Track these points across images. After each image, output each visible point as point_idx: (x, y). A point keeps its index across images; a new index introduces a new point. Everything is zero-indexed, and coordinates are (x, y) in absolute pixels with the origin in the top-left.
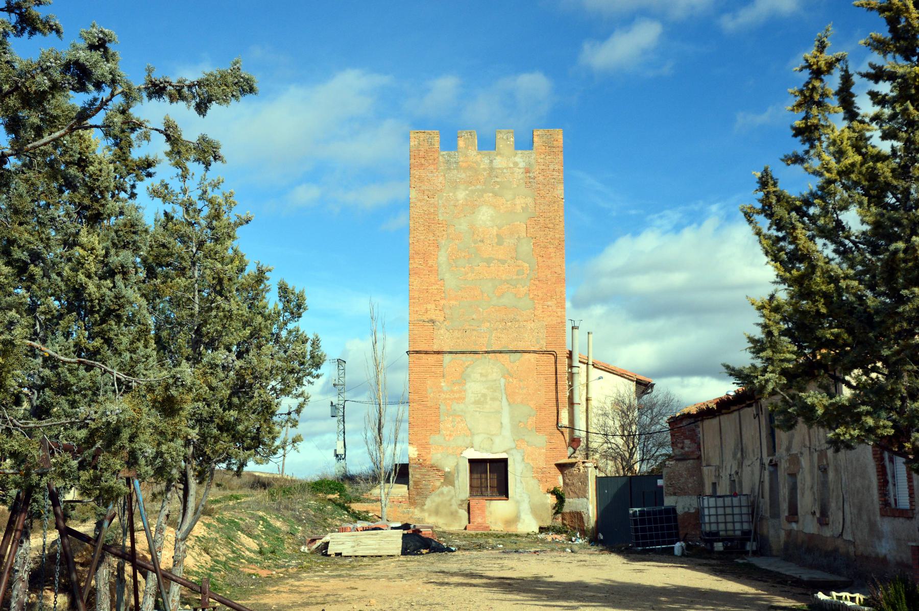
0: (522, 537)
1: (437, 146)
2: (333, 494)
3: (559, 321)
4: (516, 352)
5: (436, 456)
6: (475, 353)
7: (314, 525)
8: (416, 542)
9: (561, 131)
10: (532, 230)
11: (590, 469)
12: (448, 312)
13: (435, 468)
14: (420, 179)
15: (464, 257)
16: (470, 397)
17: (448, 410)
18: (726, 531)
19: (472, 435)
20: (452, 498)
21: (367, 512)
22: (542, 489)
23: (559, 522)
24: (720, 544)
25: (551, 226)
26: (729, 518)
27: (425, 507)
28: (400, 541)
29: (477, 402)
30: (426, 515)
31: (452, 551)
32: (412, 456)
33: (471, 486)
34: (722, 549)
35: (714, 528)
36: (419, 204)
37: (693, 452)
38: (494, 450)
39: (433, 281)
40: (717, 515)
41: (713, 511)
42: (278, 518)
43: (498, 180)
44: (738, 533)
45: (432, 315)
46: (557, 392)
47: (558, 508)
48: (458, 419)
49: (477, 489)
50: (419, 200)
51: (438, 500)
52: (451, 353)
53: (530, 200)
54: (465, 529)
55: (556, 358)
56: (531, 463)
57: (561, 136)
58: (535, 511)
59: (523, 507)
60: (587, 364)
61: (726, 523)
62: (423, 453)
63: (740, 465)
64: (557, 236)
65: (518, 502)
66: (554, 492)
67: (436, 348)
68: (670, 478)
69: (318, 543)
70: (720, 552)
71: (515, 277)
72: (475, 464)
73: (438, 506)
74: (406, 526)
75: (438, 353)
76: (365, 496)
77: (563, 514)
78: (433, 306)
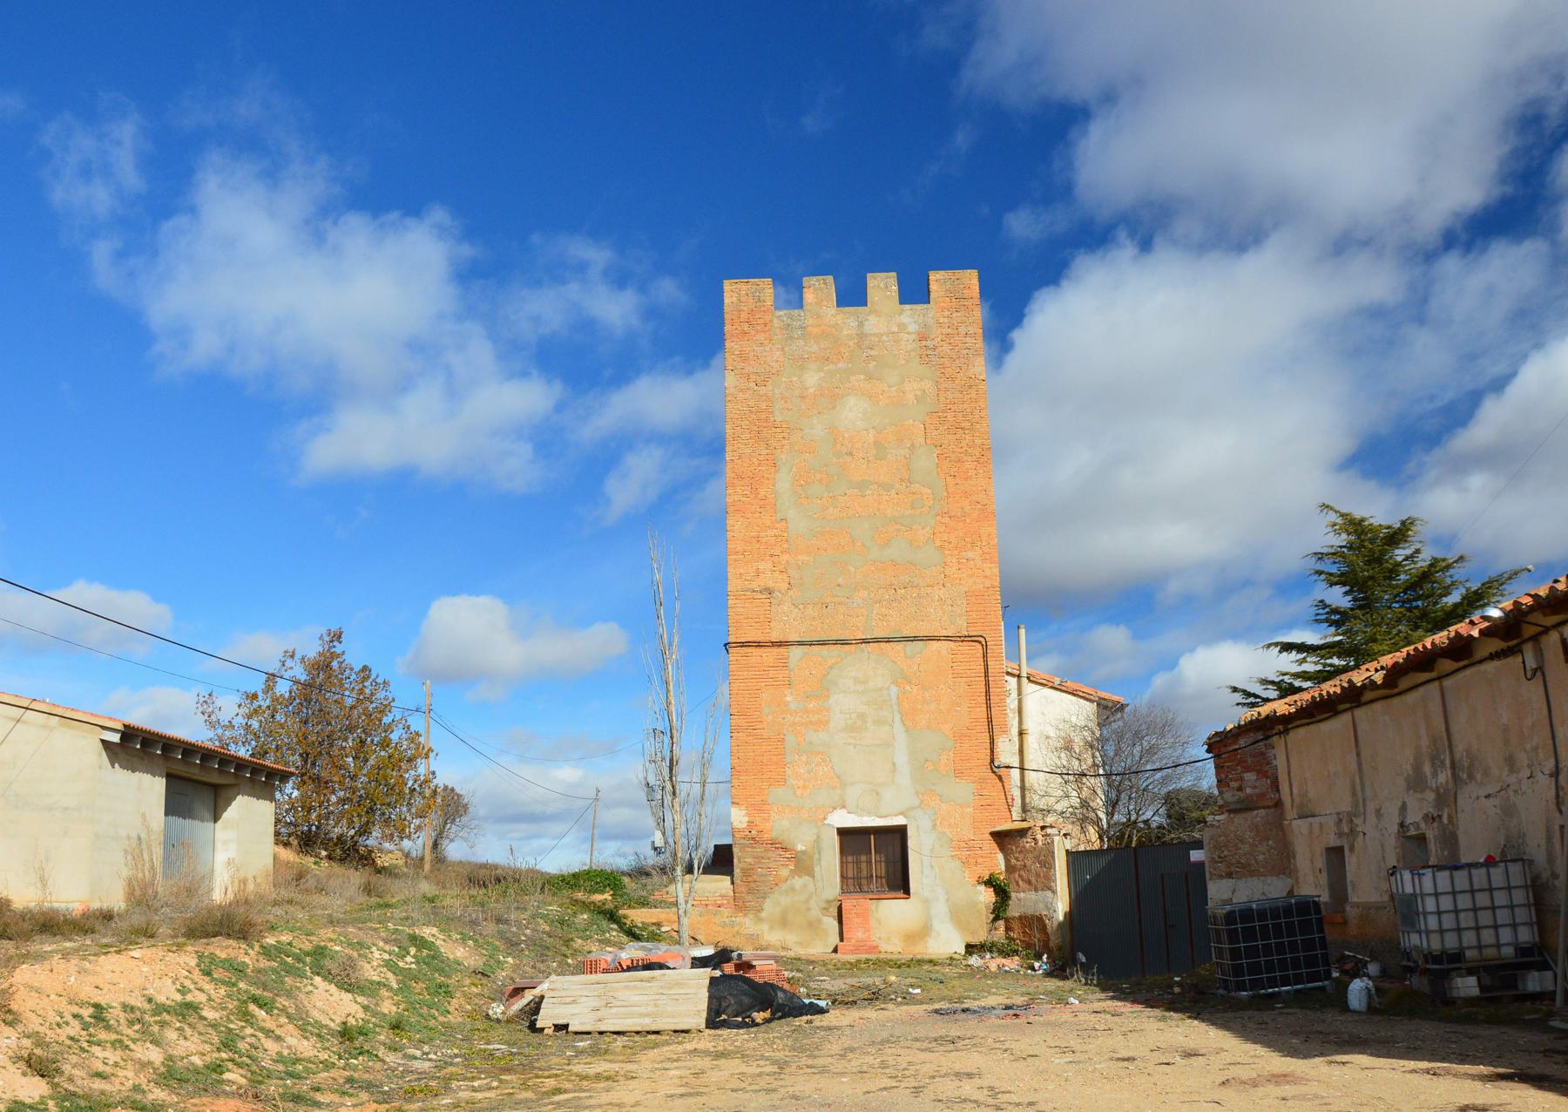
0: (942, 964)
1: (769, 301)
2: (602, 892)
4: (915, 639)
5: (778, 825)
6: (844, 642)
9: (974, 273)
11: (1056, 839)
13: (779, 846)
14: (743, 357)
18: (1480, 947)
20: (810, 897)
21: (659, 925)
22: (969, 877)
24: (1472, 981)
25: (966, 425)
26: (1485, 918)
27: (763, 915)
28: (705, 994)
30: (765, 927)
31: (822, 1011)
32: (737, 824)
34: (1476, 992)
35: (1451, 942)
37: (1262, 795)
39: (768, 523)
40: (1456, 911)
41: (1446, 903)
43: (873, 353)
44: (1508, 951)
46: (989, 707)
47: (999, 911)
49: (853, 882)
51: (785, 901)
52: (801, 643)
53: (928, 385)
54: (835, 950)
55: (985, 647)
58: (958, 917)
59: (938, 913)
60: (1019, 676)
61: (1477, 928)
63: (1445, 798)
64: (978, 441)
66: (990, 882)
68: (1218, 847)
69: (529, 996)
70: (1470, 1001)
72: (851, 838)
74: (722, 956)
75: (780, 644)
76: (657, 896)
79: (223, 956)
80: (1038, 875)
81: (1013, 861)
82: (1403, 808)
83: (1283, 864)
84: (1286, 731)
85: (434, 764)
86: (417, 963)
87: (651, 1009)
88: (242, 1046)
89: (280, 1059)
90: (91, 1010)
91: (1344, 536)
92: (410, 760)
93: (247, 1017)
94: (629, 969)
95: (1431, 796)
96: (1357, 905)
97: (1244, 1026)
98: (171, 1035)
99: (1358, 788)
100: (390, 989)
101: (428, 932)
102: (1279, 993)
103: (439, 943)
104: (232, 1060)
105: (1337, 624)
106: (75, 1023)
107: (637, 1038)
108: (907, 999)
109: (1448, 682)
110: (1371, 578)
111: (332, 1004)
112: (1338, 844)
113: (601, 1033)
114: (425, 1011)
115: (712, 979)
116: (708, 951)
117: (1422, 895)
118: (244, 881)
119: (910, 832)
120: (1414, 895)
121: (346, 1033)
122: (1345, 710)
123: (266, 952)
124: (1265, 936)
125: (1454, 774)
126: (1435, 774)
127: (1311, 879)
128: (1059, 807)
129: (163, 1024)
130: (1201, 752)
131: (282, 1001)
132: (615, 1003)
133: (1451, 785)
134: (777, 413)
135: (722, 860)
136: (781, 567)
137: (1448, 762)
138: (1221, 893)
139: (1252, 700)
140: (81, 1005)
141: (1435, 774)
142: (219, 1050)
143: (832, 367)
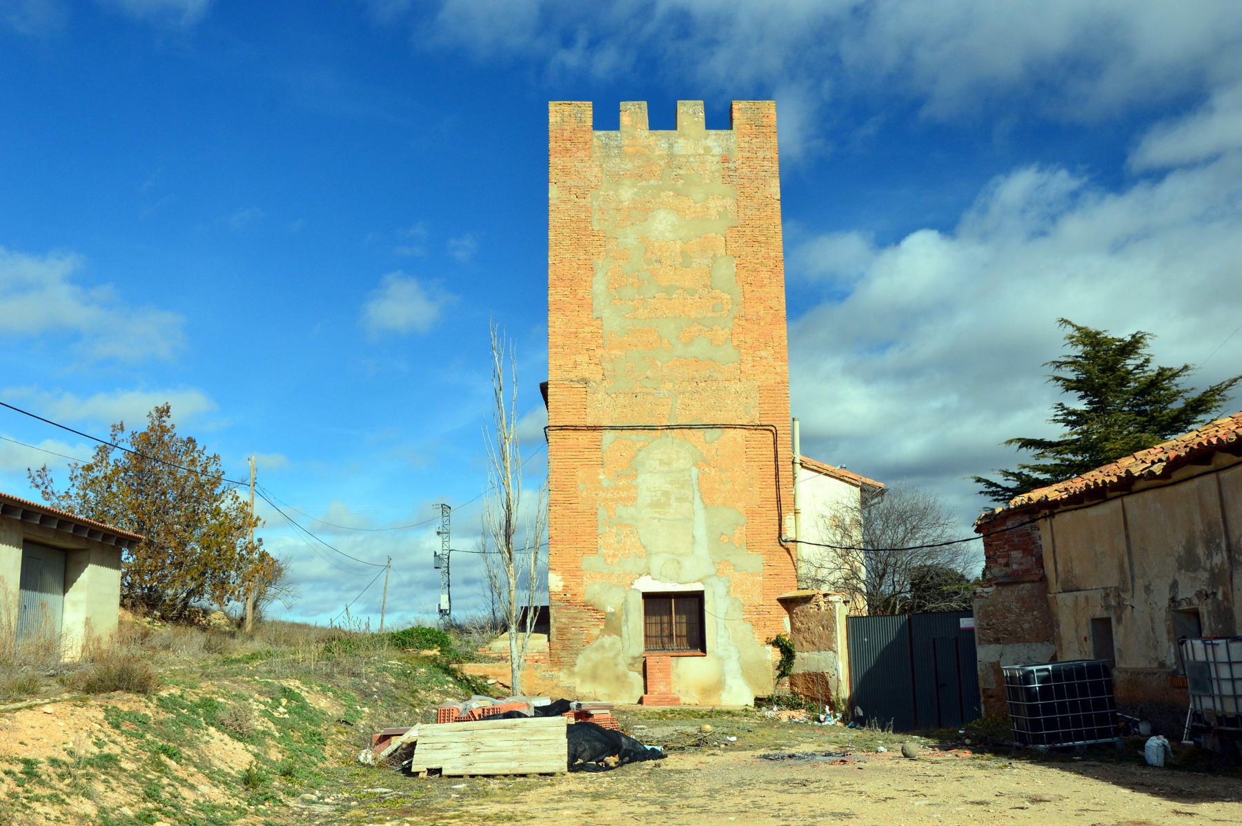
2: (430, 648)
3: (779, 379)
4: (714, 426)
5: (591, 590)
7: (394, 702)
8: (599, 745)
10: (735, 245)
11: (838, 605)
12: (608, 366)
13: (591, 608)
14: (565, 171)
15: (632, 284)
16: (644, 497)
17: (610, 517)
19: (649, 555)
20: (617, 654)
21: (485, 678)
23: (785, 689)
25: (762, 239)
27: (576, 669)
29: (655, 505)
30: (577, 681)
33: (646, 636)
36: (562, 206)
37: (1027, 571)
39: (585, 320)
42: (324, 691)
43: (681, 172)
46: (778, 488)
47: (785, 667)
49: (657, 640)
50: (565, 202)
51: (596, 656)
52: (613, 428)
53: (729, 202)
54: (641, 701)
55: (775, 435)
56: (739, 596)
57: (773, 111)
58: (748, 672)
59: (729, 669)
64: (772, 254)
65: (720, 659)
66: (777, 643)
67: (590, 422)
69: (396, 743)
71: (709, 315)
72: (655, 602)
73: (595, 667)
75: (595, 428)
76: (481, 651)
77: (792, 677)
78: (586, 359)
79: (126, 709)
80: (820, 637)
81: (798, 625)
82: (1174, 585)
83: (1047, 631)
84: (1052, 515)
85: (256, 534)
86: (289, 712)
87: (516, 754)
88: (165, 795)
89: (199, 808)
90: (21, 767)
91: (1081, 347)
92: (239, 528)
93: (160, 767)
94: (488, 718)
95: (1205, 576)
96: (1126, 671)
98: (100, 788)
99: (1127, 565)
100: (273, 737)
101: (293, 684)
102: (1073, 747)
103: (303, 694)
104: (160, 810)
105: (1073, 424)
106: (8, 779)
107: (507, 781)
108: (730, 747)
109: (1225, 475)
110: (1105, 385)
111: (233, 755)
112: (1105, 615)
113: (472, 776)
114: (306, 758)
115: (569, 726)
116: (546, 702)
117: (1215, 663)
118: (99, 640)
119: (707, 597)
120: (1207, 663)
121: (249, 780)
122: (1116, 498)
123: (162, 704)
124: (1072, 695)
125: (1230, 557)
126: (1210, 556)
127: (1075, 646)
128: (831, 578)
129: (89, 777)
130: (970, 532)
131: (186, 751)
132: (483, 748)
133: (1226, 566)
134: (595, 223)
135: (543, 621)
136: (596, 361)
137: (1223, 546)
138: (985, 654)
139: (993, 489)
140: (11, 761)
141: (1210, 556)
142: (144, 800)
143: (644, 183)
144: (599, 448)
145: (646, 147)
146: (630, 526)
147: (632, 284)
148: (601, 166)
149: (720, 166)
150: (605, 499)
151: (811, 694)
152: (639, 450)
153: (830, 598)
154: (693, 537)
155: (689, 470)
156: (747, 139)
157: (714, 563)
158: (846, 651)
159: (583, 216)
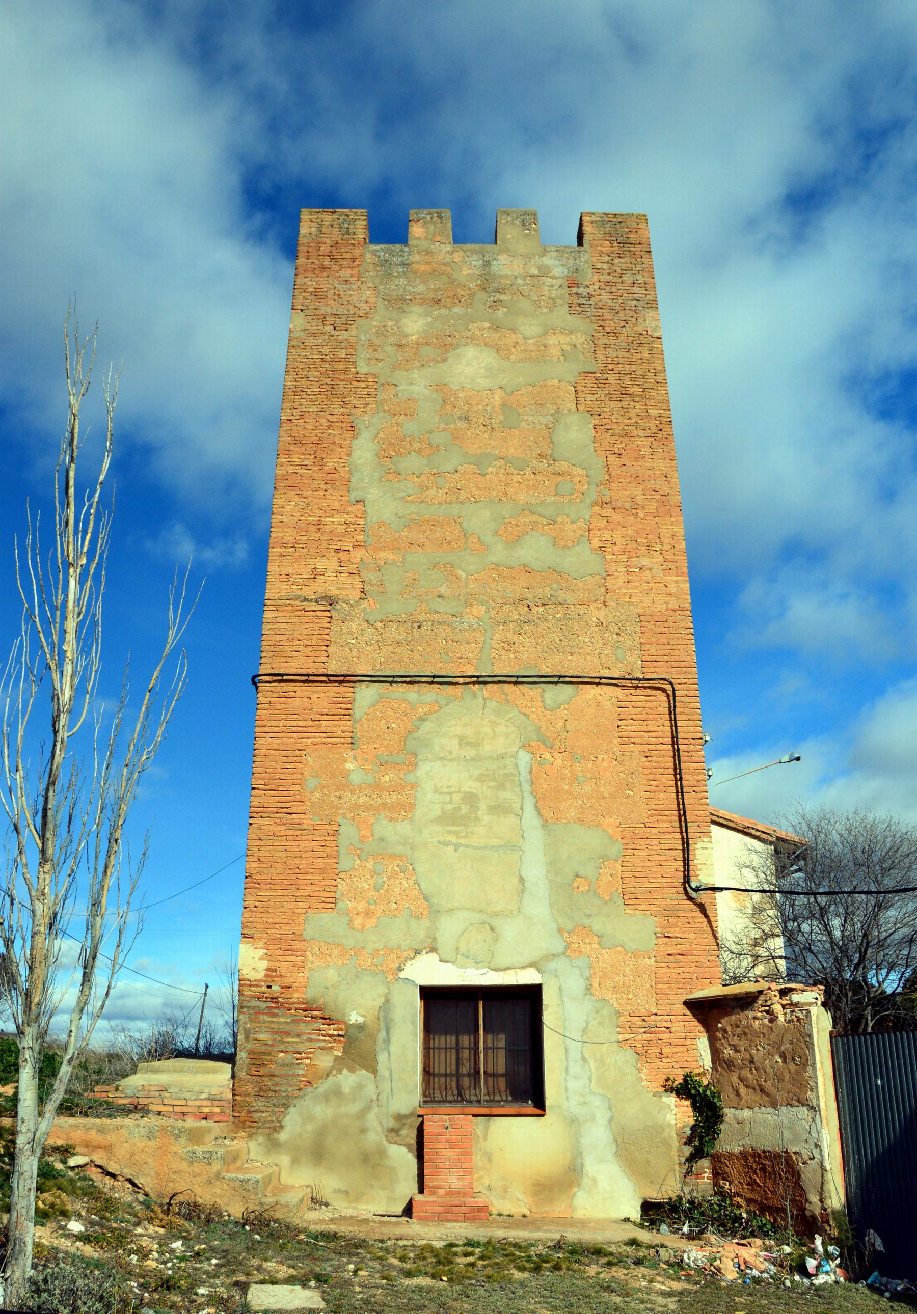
4: (559, 680)
5: (320, 978)
10: (590, 397)
13: (318, 1013)
16: (429, 802)
17: (363, 839)
19: (435, 912)
20: (367, 1109)
22: (647, 1081)
27: (283, 1136)
29: (449, 819)
36: (311, 341)
38: (502, 961)
39: (336, 505)
43: (502, 297)
45: (330, 585)
46: (680, 792)
48: (393, 866)
49: (445, 1084)
50: (314, 335)
51: (322, 1112)
52: (374, 679)
53: (579, 339)
54: (408, 1211)
55: (672, 699)
56: (609, 996)
58: (629, 1150)
62: (284, 967)
64: (654, 412)
65: (573, 1123)
66: (685, 1089)
67: (333, 668)
75: (343, 679)
77: (716, 1159)
78: (334, 564)
81: (728, 1052)
97: (94, 1053)
119: (548, 998)
143: (443, 311)
144: (348, 714)
145: (446, 265)
146: (401, 857)
147: (419, 451)
148: (375, 288)
149: (566, 291)
150: (356, 807)
151: (766, 1195)
152: (422, 719)
153: (795, 998)
154: (522, 880)
155: (515, 756)
156: (606, 258)
157: (560, 930)
158: (834, 1105)
159: (342, 354)
